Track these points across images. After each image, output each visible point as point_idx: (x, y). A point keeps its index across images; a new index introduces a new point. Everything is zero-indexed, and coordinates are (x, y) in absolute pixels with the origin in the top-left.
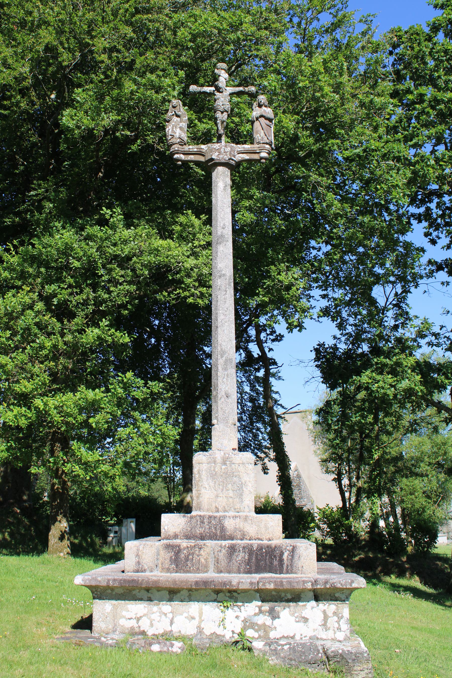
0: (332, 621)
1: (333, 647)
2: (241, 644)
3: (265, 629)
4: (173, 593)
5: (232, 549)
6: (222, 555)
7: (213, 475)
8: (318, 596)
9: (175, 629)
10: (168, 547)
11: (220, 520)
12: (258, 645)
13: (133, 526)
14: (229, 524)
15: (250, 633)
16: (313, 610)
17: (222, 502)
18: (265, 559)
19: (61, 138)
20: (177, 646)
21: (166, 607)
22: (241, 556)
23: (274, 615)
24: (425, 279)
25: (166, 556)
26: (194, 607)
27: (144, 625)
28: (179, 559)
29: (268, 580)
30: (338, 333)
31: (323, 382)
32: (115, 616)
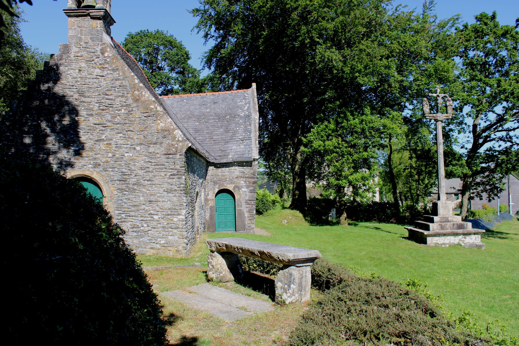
0: (477, 239)
1: (478, 244)
2: (459, 244)
3: (463, 241)
4: (444, 235)
5: (454, 225)
6: (451, 226)
7: (443, 207)
8: (474, 234)
9: (445, 242)
11: (447, 218)
12: (463, 244)
13: (335, 211)
14: (450, 219)
15: (460, 242)
16: (473, 237)
17: (445, 213)
18: (460, 227)
19: (293, 95)
20: (447, 246)
21: (443, 238)
22: (455, 226)
23: (465, 238)
24: (353, 184)
25: (439, 227)
26: (449, 237)
27: (438, 242)
28: (442, 228)
29: (460, 231)
30: (278, 206)
31: (124, 232)
32: (432, 240)
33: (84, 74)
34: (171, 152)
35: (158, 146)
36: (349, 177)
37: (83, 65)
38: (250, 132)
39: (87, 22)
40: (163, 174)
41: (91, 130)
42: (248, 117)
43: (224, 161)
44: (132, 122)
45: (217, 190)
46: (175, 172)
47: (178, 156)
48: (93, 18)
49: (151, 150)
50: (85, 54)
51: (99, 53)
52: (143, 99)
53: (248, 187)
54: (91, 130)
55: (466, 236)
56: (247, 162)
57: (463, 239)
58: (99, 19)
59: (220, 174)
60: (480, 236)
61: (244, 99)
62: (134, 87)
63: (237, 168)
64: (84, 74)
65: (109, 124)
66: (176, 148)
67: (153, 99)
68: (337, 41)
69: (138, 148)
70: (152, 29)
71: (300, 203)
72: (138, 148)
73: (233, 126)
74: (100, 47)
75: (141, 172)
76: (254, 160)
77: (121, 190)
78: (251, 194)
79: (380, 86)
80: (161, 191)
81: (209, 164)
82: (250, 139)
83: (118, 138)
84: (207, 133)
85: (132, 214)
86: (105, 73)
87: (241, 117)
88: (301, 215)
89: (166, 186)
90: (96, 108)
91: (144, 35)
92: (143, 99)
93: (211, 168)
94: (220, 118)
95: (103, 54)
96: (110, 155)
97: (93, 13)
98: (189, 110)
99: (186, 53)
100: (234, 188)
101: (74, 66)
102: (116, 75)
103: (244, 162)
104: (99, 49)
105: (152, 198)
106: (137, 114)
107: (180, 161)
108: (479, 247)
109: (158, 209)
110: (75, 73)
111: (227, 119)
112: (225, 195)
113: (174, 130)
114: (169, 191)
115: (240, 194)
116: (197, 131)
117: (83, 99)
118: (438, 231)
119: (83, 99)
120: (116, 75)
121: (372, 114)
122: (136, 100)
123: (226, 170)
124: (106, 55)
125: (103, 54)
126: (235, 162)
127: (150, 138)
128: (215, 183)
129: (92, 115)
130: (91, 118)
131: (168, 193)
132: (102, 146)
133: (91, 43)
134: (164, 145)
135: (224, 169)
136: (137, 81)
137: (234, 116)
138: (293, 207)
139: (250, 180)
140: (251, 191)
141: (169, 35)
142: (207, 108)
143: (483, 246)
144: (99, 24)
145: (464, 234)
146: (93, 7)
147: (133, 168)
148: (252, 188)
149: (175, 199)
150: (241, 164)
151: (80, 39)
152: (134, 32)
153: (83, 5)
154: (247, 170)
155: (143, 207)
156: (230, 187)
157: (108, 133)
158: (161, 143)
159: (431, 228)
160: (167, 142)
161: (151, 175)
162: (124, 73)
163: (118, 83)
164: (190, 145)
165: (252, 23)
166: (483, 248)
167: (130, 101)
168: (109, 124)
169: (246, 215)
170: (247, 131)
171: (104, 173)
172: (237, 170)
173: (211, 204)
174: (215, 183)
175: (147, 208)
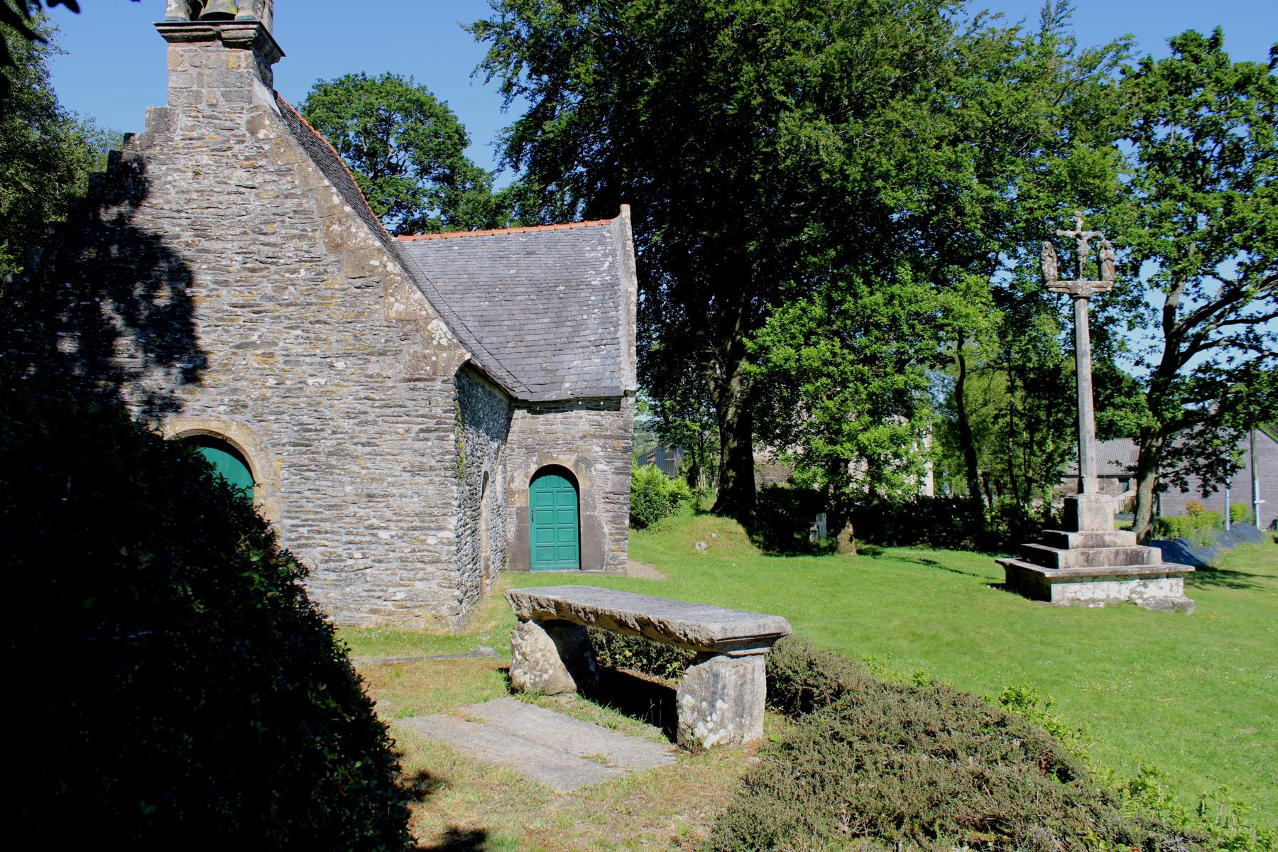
0: (1175, 588)
1: (1177, 600)
2: (1130, 601)
3: (1141, 593)
4: (1094, 578)
5: (1117, 553)
6: (1112, 556)
7: (1090, 510)
8: (1168, 576)
9: (1095, 596)
10: (1083, 553)
11: (1102, 536)
12: (1139, 601)
13: (824, 518)
14: (1107, 539)
15: (1134, 596)
16: (1165, 583)
17: (1095, 525)
18: (1134, 558)
20: (1102, 605)
21: (1090, 585)
22: (1122, 557)
23: (1145, 586)
25: (1081, 558)
26: (1105, 584)
27: (1079, 595)
28: (1089, 561)
29: (1134, 569)
31: (304, 572)
32: (1063, 592)
33: (206, 182)
34: (422, 374)
35: (389, 359)
36: (860, 437)
37: (205, 159)
38: (616, 326)
39: (214, 53)
40: (400, 428)
41: (224, 319)
42: (611, 287)
43: (552, 396)
44: (324, 301)
45: (533, 469)
46: (431, 423)
47: (438, 385)
48: (229, 44)
49: (373, 369)
50: (208, 132)
51: (243, 130)
52: (351, 243)
53: (610, 460)
54: (224, 319)
55: (1148, 582)
56: (608, 399)
57: (1141, 589)
58: (244, 46)
59: (541, 428)
60: (1181, 582)
61: (601, 243)
62: (330, 215)
63: (583, 413)
64: (206, 182)
65: (268, 305)
66: (435, 365)
67: (378, 244)
68: (829, 101)
69: (340, 365)
70: (375, 72)
71: (740, 500)
72: (340, 365)
73: (574, 309)
74: (246, 117)
75: (347, 424)
76: (626, 394)
77: (298, 468)
78: (617, 478)
79: (935, 213)
80: (397, 469)
81: (515, 403)
82: (615, 341)
83: (290, 341)
84: (510, 328)
85: (326, 526)
86: (259, 179)
87: (594, 288)
88: (741, 530)
89: (408, 458)
90: (237, 266)
91: (354, 86)
92: (351, 243)
93: (519, 414)
94: (542, 290)
95: (253, 132)
96: (272, 381)
97: (230, 31)
98: (465, 272)
99: (457, 131)
100: (577, 463)
101: (182, 161)
102: (284, 184)
103: (600, 399)
104: (243, 119)
105: (375, 488)
106: (338, 280)
107: (443, 396)
108: (1179, 608)
109: (388, 514)
110: (184, 180)
111: (558, 292)
112: (554, 479)
113: (428, 319)
114: (415, 471)
115: (591, 479)
116: (484, 322)
117: (204, 244)
118: (1078, 569)
119: (204, 244)
120: (284, 184)
121: (916, 280)
122: (336, 247)
123: (556, 418)
124: (261, 135)
125: (253, 132)
126: (578, 399)
127: (369, 339)
128: (530, 450)
129: (226, 283)
130: (224, 292)
131: (414, 474)
132: (252, 359)
133: (223, 105)
134: (405, 357)
135: (551, 416)
136: (336, 200)
137: (576, 286)
138: (721, 509)
139: (616, 443)
140: (618, 471)
141: (416, 86)
142: (509, 267)
143: (1189, 605)
144: (244, 58)
145: (1143, 577)
146: (228, 17)
147: (327, 413)
148: (619, 464)
149: (431, 490)
150: (593, 403)
151: (198, 96)
152: (329, 78)
153: (203, 12)
154: (607, 418)
155: (352, 509)
156: (567, 461)
157: (265, 328)
158: (397, 353)
159: (1061, 563)
160: (410, 349)
161: (372, 430)
162: (305, 179)
163: (290, 204)
164: (468, 356)
165: (620, 58)
166: (1190, 612)
167: (320, 249)
168: (268, 305)
169: (607, 529)
170: (609, 322)
171: (256, 427)
172: (583, 419)
173: (520, 501)
174: (530, 450)
175: (361, 512)
